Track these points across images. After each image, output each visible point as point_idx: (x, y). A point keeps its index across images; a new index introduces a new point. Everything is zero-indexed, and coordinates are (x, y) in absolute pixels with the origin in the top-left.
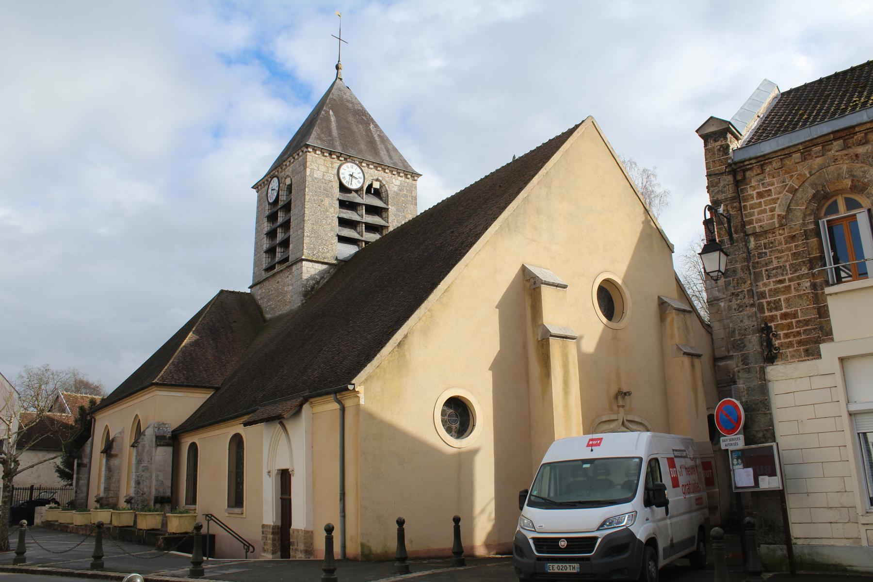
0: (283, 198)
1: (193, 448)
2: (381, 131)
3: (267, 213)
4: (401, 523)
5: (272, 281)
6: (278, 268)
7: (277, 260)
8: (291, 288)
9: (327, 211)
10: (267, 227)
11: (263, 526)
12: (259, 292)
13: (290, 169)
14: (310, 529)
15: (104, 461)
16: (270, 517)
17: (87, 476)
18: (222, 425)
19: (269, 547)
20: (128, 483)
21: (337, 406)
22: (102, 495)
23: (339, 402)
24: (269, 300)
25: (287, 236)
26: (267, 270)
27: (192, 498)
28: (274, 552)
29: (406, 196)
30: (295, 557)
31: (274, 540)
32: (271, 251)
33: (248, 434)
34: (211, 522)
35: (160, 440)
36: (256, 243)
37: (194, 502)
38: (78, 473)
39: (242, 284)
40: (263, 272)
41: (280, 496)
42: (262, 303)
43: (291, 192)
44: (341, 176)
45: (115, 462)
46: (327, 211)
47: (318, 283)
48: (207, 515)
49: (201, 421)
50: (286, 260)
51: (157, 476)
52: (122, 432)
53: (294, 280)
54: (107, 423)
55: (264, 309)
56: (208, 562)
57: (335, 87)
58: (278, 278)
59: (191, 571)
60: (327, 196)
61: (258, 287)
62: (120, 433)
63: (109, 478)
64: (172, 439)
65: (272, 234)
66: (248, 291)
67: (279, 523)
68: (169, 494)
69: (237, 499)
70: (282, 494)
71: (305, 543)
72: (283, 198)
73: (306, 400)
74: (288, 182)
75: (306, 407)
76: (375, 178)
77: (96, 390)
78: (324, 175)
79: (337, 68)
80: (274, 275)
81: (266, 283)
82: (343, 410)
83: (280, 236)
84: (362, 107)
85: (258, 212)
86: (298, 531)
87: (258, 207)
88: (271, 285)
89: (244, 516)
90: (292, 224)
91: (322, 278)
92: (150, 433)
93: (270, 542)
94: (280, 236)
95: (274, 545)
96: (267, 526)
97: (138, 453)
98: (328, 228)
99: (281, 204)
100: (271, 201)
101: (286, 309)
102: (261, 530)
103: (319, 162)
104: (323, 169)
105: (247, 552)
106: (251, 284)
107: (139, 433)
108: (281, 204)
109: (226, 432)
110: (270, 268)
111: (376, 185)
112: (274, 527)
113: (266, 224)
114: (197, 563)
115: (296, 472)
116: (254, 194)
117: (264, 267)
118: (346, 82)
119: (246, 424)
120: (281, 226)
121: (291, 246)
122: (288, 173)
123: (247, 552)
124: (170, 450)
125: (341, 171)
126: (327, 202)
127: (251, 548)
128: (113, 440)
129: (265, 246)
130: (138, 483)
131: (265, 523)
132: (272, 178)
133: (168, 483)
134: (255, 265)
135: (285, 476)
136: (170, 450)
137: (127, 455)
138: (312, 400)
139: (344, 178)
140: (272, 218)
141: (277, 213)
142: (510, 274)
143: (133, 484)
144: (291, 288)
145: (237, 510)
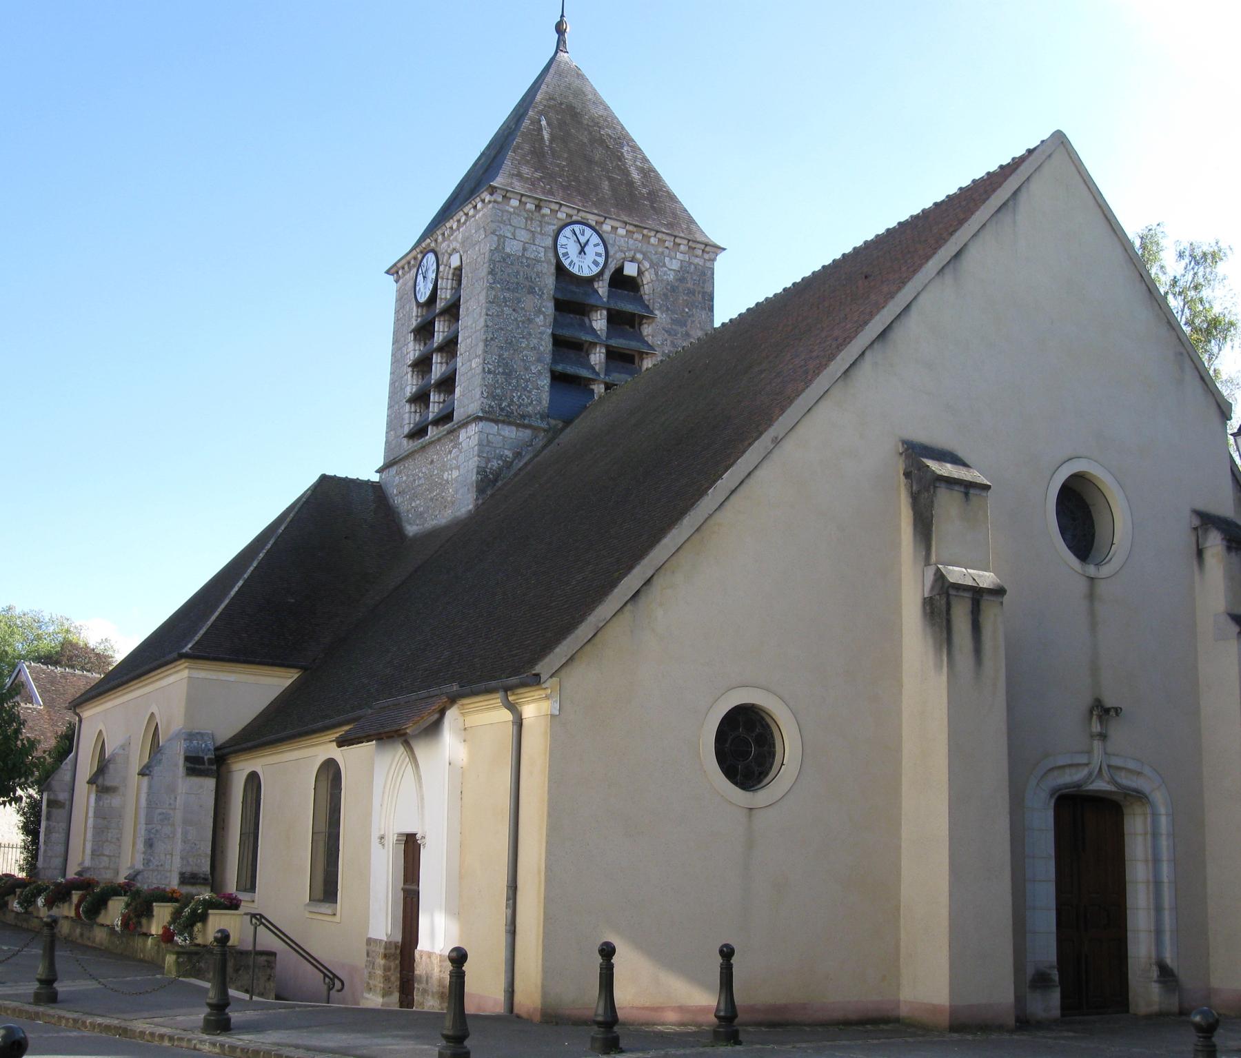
0: (445, 295)
1: (253, 779)
2: (645, 160)
3: (414, 324)
6: (432, 432)
7: (431, 416)
8: (455, 474)
10: (413, 351)
11: (369, 941)
12: (396, 483)
13: (459, 236)
14: (60, 997)
15: (93, 797)
16: (383, 925)
17: (63, 825)
18: (267, 751)
19: (378, 983)
20: (134, 844)
21: (507, 715)
22: (87, 863)
23: (512, 707)
24: (412, 499)
25: (451, 366)
26: (412, 435)
27: (249, 882)
28: (386, 994)
29: (691, 292)
30: (422, 1004)
31: (386, 969)
32: (421, 398)
33: (352, 759)
34: (261, 929)
35: (195, 765)
36: (392, 383)
37: (252, 888)
38: (48, 819)
39: (362, 461)
40: (405, 441)
42: (400, 502)
43: (460, 283)
44: (561, 251)
45: (114, 801)
46: (530, 321)
47: (508, 465)
48: (253, 916)
49: (275, 727)
51: (185, 834)
52: (125, 746)
53: (461, 458)
54: (101, 727)
55: (403, 515)
56: (244, 1005)
57: (552, 71)
58: (432, 454)
59: (206, 1021)
60: (531, 291)
61: (394, 470)
62: (123, 747)
63: (100, 831)
64: (210, 762)
65: (422, 365)
66: (375, 478)
68: (206, 868)
69: (327, 888)
70: (405, 881)
72: (445, 295)
73: (453, 700)
74: (455, 261)
75: (452, 715)
77: (101, 658)
78: (524, 249)
79: (560, 29)
80: (423, 448)
81: (409, 464)
82: (519, 723)
83: (438, 369)
84: (607, 108)
85: (397, 320)
86: (430, 955)
87: (397, 312)
88: (418, 469)
89: (337, 919)
90: (461, 347)
91: (518, 455)
92: (176, 754)
93: (379, 972)
94: (438, 369)
95: (387, 979)
96: (375, 940)
97: (150, 787)
98: (532, 356)
99: (440, 305)
100: (422, 299)
101: (442, 518)
102: (364, 948)
103: (515, 222)
104: (523, 235)
105: (330, 989)
106: (380, 463)
107: (156, 748)
108: (440, 305)
109: (324, 749)
110: (418, 432)
111: (630, 270)
112: (388, 945)
113: (411, 345)
114: (221, 1006)
115: (427, 841)
116: (390, 287)
117: (406, 430)
118: (573, 57)
119: (341, 743)
120: (440, 349)
121: (457, 390)
122: (455, 245)
123: (330, 989)
124: (210, 783)
125: (562, 240)
126: (529, 302)
127: (338, 984)
128: (113, 756)
129: (410, 390)
130: (149, 844)
131: (372, 935)
134: (392, 425)
135: (411, 846)
136: (210, 783)
137: (133, 793)
138: (465, 701)
139: (566, 254)
140: (424, 331)
141: (432, 323)
142: (882, 458)
143: (141, 846)
144: (455, 474)
145: (326, 908)
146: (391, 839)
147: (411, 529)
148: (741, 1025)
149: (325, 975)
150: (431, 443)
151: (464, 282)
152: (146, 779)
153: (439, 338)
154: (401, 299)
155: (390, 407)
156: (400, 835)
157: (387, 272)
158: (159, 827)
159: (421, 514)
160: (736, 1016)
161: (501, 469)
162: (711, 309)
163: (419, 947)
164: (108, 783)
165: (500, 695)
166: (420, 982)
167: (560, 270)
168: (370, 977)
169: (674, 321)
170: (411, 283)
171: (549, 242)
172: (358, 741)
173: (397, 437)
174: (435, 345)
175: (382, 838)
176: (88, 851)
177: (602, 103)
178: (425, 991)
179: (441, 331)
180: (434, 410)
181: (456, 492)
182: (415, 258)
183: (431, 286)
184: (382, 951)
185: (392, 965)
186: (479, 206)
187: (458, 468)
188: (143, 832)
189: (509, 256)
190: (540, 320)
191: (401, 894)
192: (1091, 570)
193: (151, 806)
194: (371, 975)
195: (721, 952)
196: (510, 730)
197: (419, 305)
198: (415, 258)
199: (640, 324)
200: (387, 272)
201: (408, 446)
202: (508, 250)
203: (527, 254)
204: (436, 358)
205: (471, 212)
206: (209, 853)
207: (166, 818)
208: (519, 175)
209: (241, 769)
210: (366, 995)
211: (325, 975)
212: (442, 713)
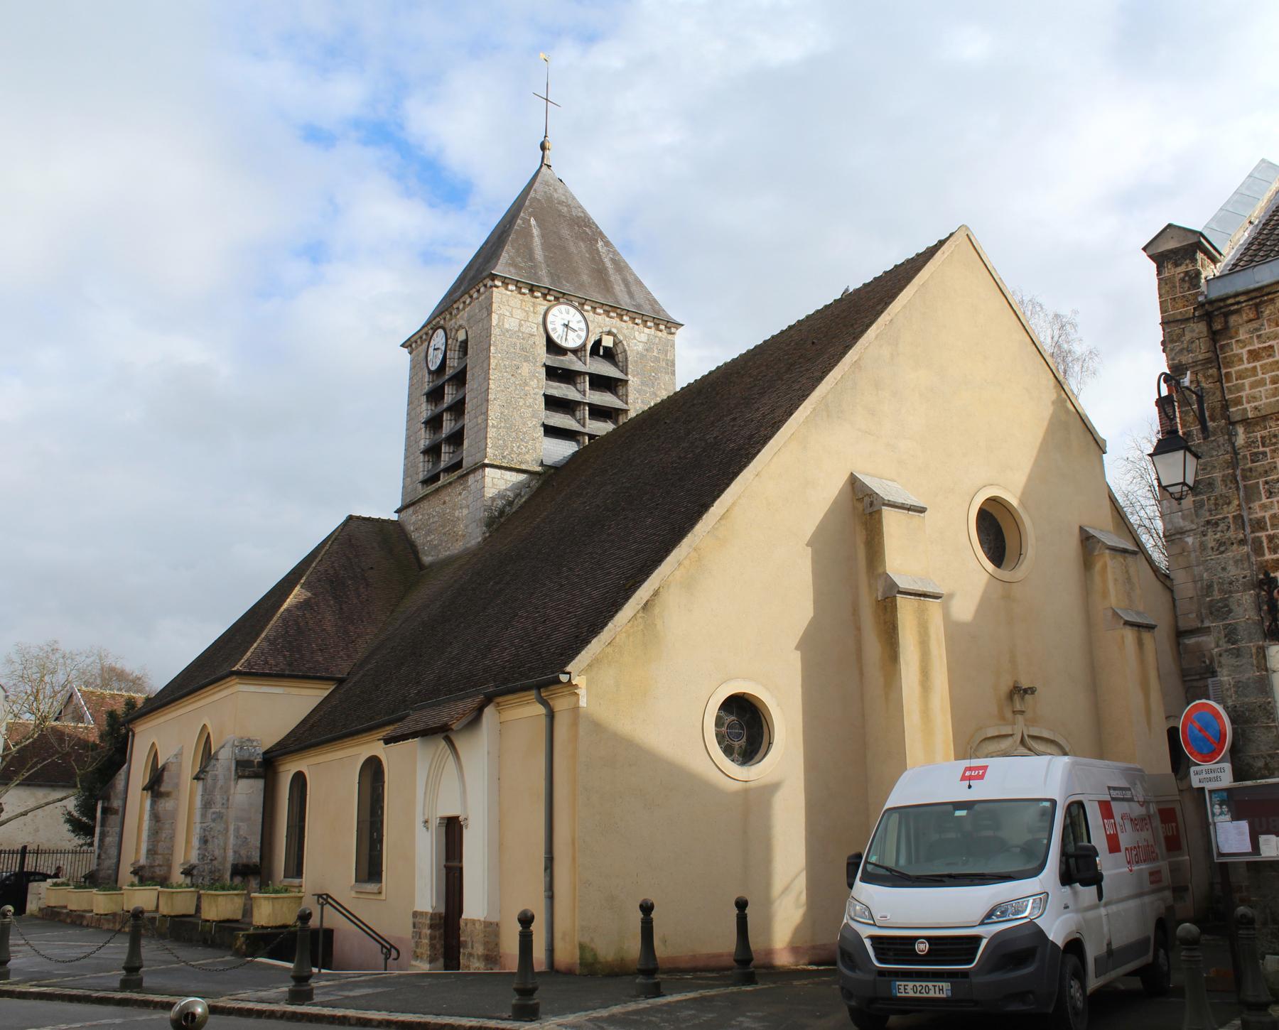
0: (453, 364)
1: (299, 781)
4: (647, 908)
5: (434, 501)
6: (443, 479)
8: (465, 512)
9: (526, 384)
10: (425, 411)
11: (415, 914)
12: (412, 520)
15: (148, 803)
16: (427, 899)
17: (117, 829)
18: (312, 752)
19: (425, 950)
20: (188, 842)
21: (540, 710)
22: (143, 861)
23: (544, 703)
24: (429, 532)
26: (426, 482)
27: (296, 868)
29: (657, 360)
30: (468, 967)
31: (432, 938)
33: (393, 757)
34: (327, 907)
35: (244, 768)
36: (408, 438)
38: (103, 825)
39: (382, 504)
40: (420, 486)
41: (444, 863)
44: (550, 327)
45: (166, 805)
46: (526, 384)
47: (510, 503)
49: (312, 735)
50: (459, 465)
51: (237, 829)
52: (179, 755)
53: (471, 499)
55: (420, 548)
56: (319, 975)
58: (444, 496)
59: (291, 992)
60: (526, 360)
61: (410, 510)
63: (155, 834)
64: (264, 767)
65: (434, 423)
66: (395, 517)
67: (442, 910)
68: (256, 858)
69: (370, 867)
70: (447, 859)
71: (486, 944)
73: (489, 700)
74: (461, 336)
75: (489, 711)
76: (607, 329)
78: (520, 325)
80: (437, 491)
81: (425, 504)
82: (551, 716)
83: (448, 426)
84: (584, 212)
85: (411, 386)
86: (473, 922)
87: (411, 379)
88: (432, 509)
90: (468, 407)
92: (225, 757)
93: (426, 941)
94: (448, 426)
95: (432, 946)
96: (421, 914)
97: (205, 789)
99: (449, 372)
100: (433, 368)
101: (457, 548)
102: (410, 920)
103: (512, 303)
104: (519, 314)
105: (386, 959)
107: (208, 756)
108: (449, 372)
109: (374, 747)
111: (608, 342)
112: (433, 916)
113: (424, 406)
117: (421, 477)
120: (449, 409)
122: (461, 322)
123: (386, 959)
124: (260, 783)
125: (550, 318)
126: (525, 369)
127: (394, 953)
130: (204, 841)
131: (418, 908)
132: (434, 330)
133: (256, 841)
135: (453, 829)
136: (260, 783)
137: (186, 795)
138: (500, 699)
139: (554, 329)
140: (435, 395)
141: (442, 387)
142: (830, 488)
143: (196, 842)
144: (465, 512)
145: (371, 887)
146: (434, 823)
147: (427, 559)
148: (756, 967)
149: (383, 946)
150: (444, 486)
151: (470, 352)
152: (201, 783)
153: (448, 399)
154: (414, 367)
155: (406, 458)
156: (442, 818)
157: (403, 346)
158: (213, 825)
159: (436, 546)
160: (751, 960)
161: (504, 506)
162: (673, 373)
163: (464, 916)
164: (163, 789)
165: (534, 692)
166: (465, 947)
167: (550, 341)
168: (417, 946)
169: (643, 383)
170: (423, 354)
171: (540, 319)
172: (403, 737)
173: (413, 482)
174: (445, 406)
175: (426, 822)
176: (144, 847)
177: (580, 207)
178: (471, 955)
179: (449, 396)
180: (445, 460)
181: (466, 527)
182: (427, 334)
183: (441, 356)
184: (428, 922)
185: (437, 933)
186: (482, 290)
187: (468, 507)
188: (198, 830)
189: (507, 331)
190: (534, 383)
191: (444, 871)
192: (1004, 574)
193: (207, 805)
194: (417, 944)
195: (641, 907)
196: (543, 722)
197: (430, 372)
198: (427, 334)
199: (616, 386)
200: (403, 346)
201: (421, 491)
202: (507, 326)
203: (523, 329)
204: (446, 416)
205: (475, 295)
206: (258, 844)
207: (219, 817)
208: (515, 265)
209: (288, 771)
210: (414, 963)
211: (383, 946)
212: (480, 710)
